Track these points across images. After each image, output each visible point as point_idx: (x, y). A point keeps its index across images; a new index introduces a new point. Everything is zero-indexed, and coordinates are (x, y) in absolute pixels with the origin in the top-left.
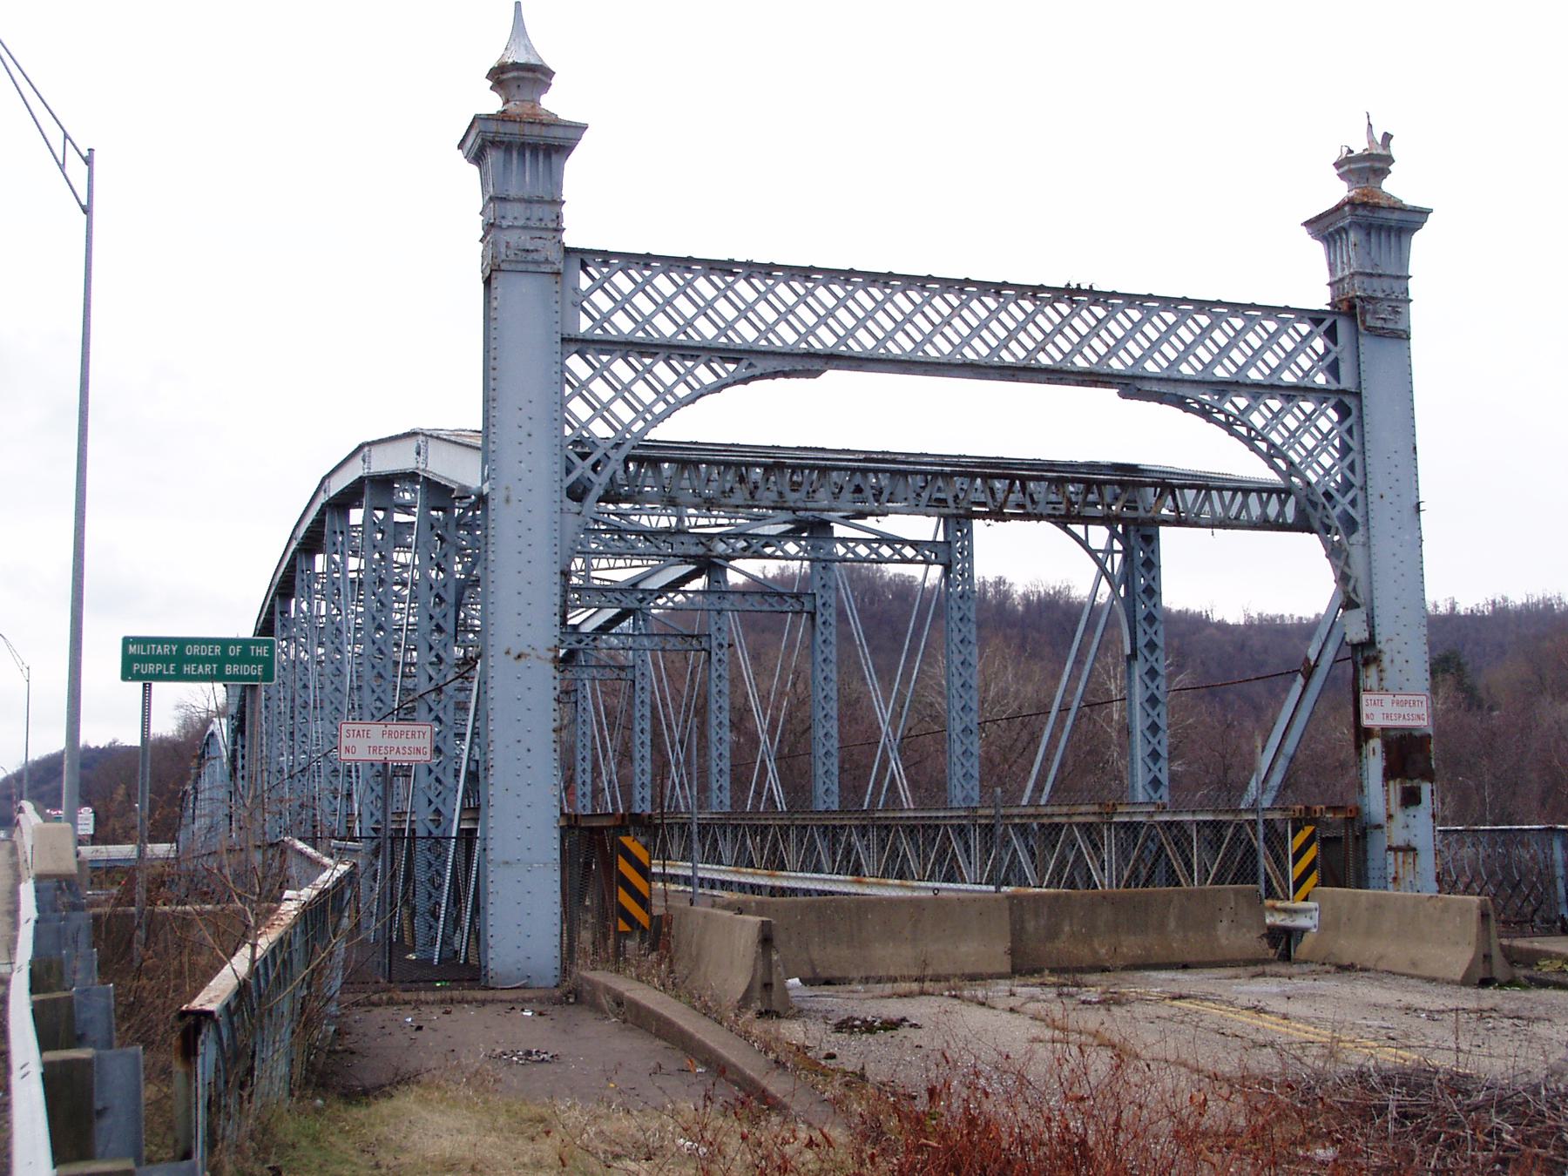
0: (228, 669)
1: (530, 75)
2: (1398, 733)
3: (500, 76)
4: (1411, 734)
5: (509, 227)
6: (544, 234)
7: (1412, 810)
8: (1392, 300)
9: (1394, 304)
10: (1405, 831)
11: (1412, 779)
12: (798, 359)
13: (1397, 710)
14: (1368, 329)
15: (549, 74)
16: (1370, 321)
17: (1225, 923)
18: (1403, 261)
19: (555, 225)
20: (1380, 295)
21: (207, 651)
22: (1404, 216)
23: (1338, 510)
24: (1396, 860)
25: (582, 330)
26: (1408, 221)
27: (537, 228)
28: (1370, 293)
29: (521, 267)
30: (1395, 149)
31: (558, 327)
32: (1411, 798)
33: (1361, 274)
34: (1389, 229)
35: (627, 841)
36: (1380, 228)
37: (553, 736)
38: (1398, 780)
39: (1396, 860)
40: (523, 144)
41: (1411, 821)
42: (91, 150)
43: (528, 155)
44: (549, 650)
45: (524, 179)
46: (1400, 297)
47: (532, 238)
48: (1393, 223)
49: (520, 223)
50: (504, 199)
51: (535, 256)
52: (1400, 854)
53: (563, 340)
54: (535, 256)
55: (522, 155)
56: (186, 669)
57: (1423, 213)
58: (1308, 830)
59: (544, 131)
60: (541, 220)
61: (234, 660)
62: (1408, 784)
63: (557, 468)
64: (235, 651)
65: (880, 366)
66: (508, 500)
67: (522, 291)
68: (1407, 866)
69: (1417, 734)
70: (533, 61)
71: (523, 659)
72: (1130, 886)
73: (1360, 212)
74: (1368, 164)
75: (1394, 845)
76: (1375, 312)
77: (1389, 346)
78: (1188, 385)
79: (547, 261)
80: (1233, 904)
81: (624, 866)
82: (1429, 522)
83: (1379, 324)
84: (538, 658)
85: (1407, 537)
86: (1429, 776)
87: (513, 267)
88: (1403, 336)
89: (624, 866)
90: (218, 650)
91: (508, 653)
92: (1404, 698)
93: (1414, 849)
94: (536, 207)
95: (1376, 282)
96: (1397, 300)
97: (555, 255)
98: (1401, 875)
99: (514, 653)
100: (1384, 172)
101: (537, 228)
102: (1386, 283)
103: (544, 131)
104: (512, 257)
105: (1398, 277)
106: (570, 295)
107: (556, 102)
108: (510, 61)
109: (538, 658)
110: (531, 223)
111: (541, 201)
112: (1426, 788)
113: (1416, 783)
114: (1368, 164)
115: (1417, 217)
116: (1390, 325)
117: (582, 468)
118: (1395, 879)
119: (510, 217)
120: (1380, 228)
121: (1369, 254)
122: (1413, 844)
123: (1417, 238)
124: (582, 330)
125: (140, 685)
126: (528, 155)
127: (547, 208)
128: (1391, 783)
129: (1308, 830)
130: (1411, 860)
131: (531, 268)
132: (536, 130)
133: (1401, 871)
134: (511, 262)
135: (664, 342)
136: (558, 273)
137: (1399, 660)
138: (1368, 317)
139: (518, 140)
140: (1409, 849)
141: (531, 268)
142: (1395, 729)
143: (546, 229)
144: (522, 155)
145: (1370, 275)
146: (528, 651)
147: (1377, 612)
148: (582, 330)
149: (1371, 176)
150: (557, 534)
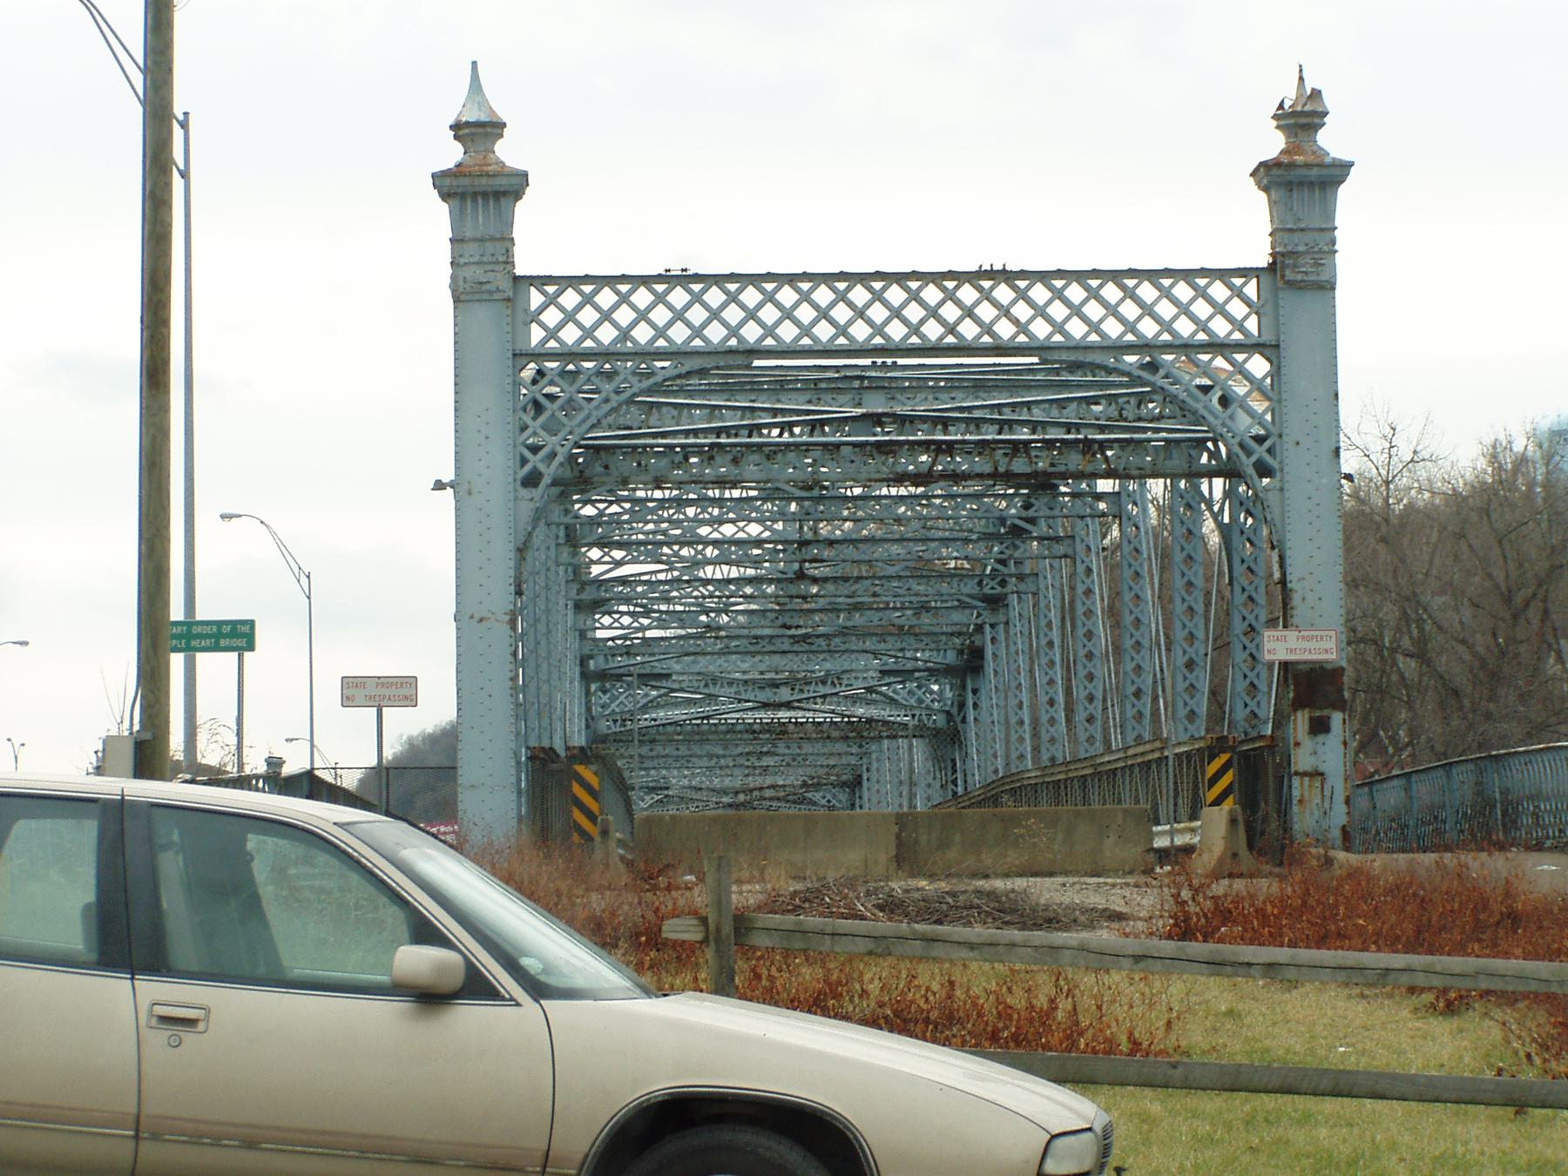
0: (223, 643)
1: (480, 130)
2: (1308, 667)
3: (461, 130)
5: (466, 264)
6: (497, 268)
7: (1321, 738)
8: (1314, 252)
9: (1317, 256)
10: (1313, 758)
11: (1321, 709)
12: (721, 356)
13: (1302, 644)
14: (1289, 283)
15: (504, 125)
16: (1289, 275)
17: (1112, 839)
18: (1329, 214)
19: (504, 259)
20: (1301, 248)
21: (208, 630)
22: (1324, 172)
23: (1253, 459)
24: (1302, 785)
25: (533, 345)
26: (1338, 172)
27: (490, 263)
28: (1290, 248)
29: (477, 297)
30: (1328, 100)
31: (509, 346)
32: (1320, 727)
33: (1281, 230)
34: (1311, 184)
35: (580, 769)
36: (1301, 184)
37: (510, 683)
38: (1307, 711)
39: (1302, 785)
40: (475, 193)
41: (1320, 749)
42: (186, 114)
43: (480, 201)
44: (505, 614)
45: (480, 222)
46: (1326, 248)
47: (485, 272)
48: (1313, 179)
49: (476, 259)
50: (462, 241)
51: (487, 287)
52: (1306, 779)
53: (514, 355)
54: (487, 287)
55: (475, 201)
56: (193, 643)
57: (1346, 167)
58: (1224, 757)
59: (491, 181)
60: (493, 255)
61: (225, 636)
62: (1318, 713)
63: (511, 463)
64: (227, 629)
65: (799, 355)
66: (470, 493)
67: (483, 314)
68: (1314, 791)
69: (1329, 667)
70: (484, 118)
71: (484, 622)
72: (1051, 805)
73: (1275, 172)
74: (1292, 121)
75: (1301, 770)
76: (1295, 266)
77: (1310, 300)
78: (1098, 351)
79: (498, 290)
80: (1120, 822)
81: (577, 790)
82: (452, 608)
83: (1299, 277)
84: (497, 620)
85: (1325, 481)
86: (1340, 705)
87: (467, 297)
88: (1329, 287)
89: (577, 790)
90: (215, 629)
91: (472, 617)
92: (1315, 633)
93: (1322, 774)
94: (487, 244)
95: (1296, 236)
96: (1320, 251)
97: (505, 284)
99: (477, 617)
100: (1316, 127)
101: (490, 263)
102: (1308, 238)
103: (491, 181)
104: (468, 289)
105: (1322, 230)
106: (521, 316)
107: (508, 152)
108: (464, 120)
109: (497, 620)
110: (485, 259)
111: (493, 239)
112: (1337, 718)
113: (1326, 712)
114: (1292, 121)
115: (1337, 171)
116: (1311, 278)
117: (535, 460)
118: (1301, 801)
119: (467, 255)
120: (1301, 184)
121: (1291, 210)
122: (1321, 769)
123: (1343, 190)
124: (533, 345)
125: (236, 654)
126: (480, 201)
127: (498, 244)
128: (1299, 714)
129: (1224, 757)
130: (1318, 784)
131: (485, 296)
132: (484, 181)
133: (1307, 794)
134: (467, 293)
135: (602, 350)
136: (508, 300)
137: (1310, 597)
138: (1287, 272)
139: (470, 190)
140: (1317, 774)
141: (485, 296)
142: (1305, 662)
143: (497, 263)
144: (475, 201)
145: (1291, 230)
146: (486, 615)
147: (1288, 553)
148: (534, 341)
149: (1299, 132)
150: (511, 518)
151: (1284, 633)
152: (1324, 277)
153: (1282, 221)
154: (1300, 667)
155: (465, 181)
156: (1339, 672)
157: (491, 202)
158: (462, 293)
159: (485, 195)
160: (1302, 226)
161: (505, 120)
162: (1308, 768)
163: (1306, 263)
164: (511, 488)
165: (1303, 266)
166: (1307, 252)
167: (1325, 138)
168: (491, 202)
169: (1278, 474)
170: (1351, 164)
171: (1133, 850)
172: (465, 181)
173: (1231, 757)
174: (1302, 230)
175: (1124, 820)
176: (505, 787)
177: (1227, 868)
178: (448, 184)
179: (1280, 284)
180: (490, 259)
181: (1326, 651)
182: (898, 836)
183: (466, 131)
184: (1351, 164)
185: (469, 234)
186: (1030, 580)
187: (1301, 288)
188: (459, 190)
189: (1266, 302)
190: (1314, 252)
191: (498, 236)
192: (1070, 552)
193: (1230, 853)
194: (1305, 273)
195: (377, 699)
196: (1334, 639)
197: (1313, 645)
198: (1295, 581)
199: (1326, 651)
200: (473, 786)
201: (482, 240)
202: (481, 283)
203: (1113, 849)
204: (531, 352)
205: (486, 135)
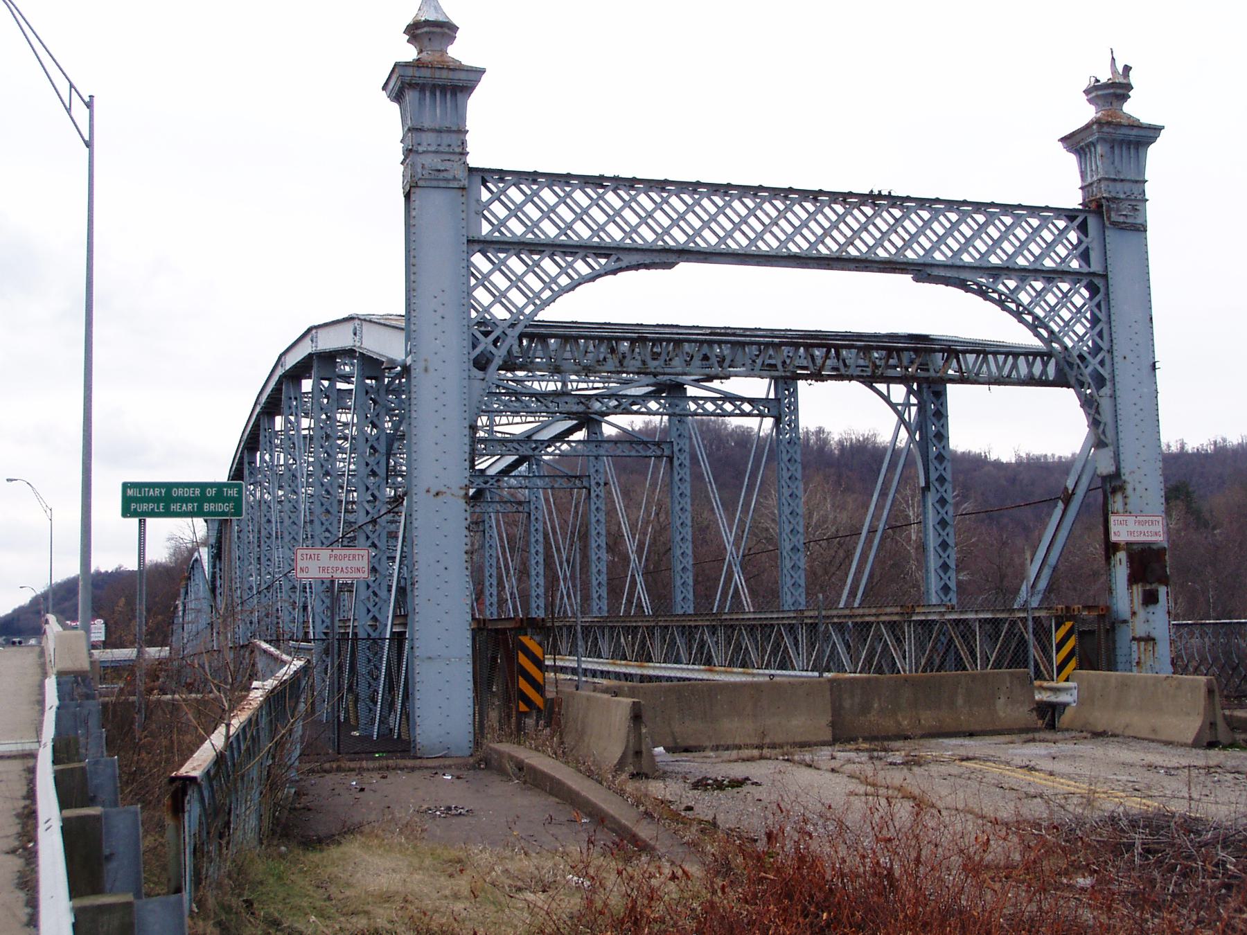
1: (438, 30)
2: (1140, 547)
4: (1149, 548)
5: (424, 152)
6: (452, 157)
7: (1151, 608)
8: (1131, 200)
9: (1134, 203)
10: (1146, 626)
11: (1151, 584)
13: (1138, 528)
14: (1114, 224)
16: (1114, 217)
17: (1002, 700)
19: (460, 150)
20: (1122, 196)
21: (189, 493)
22: (1142, 133)
24: (1139, 648)
26: (1149, 134)
28: (1114, 194)
29: (435, 183)
32: (1150, 599)
37: (465, 557)
38: (1140, 585)
39: (1139, 648)
41: (1151, 617)
43: (438, 94)
45: (434, 114)
50: (420, 130)
51: (445, 174)
54: (445, 174)
55: (433, 94)
56: (173, 507)
58: (1068, 625)
59: (451, 75)
60: (449, 146)
64: (211, 492)
65: (730, 259)
66: (426, 370)
67: (435, 202)
69: (1155, 547)
71: (440, 497)
74: (1112, 91)
75: (1138, 636)
77: (1131, 237)
79: (455, 179)
80: (1008, 685)
81: (523, 660)
83: (1121, 219)
86: (1164, 581)
88: (1141, 229)
89: (523, 660)
90: (198, 491)
91: (428, 491)
94: (444, 135)
95: (1119, 185)
96: (1136, 200)
97: (461, 174)
98: (1142, 661)
99: (433, 491)
100: (1125, 97)
102: (1127, 186)
103: (451, 75)
104: (427, 176)
108: (423, 19)
110: (441, 149)
111: (449, 131)
112: (1162, 590)
113: (1154, 586)
116: (1130, 220)
117: (485, 343)
121: (1113, 163)
126: (438, 94)
127: (454, 136)
128: (1135, 587)
130: (1151, 648)
131: (442, 184)
133: (1142, 656)
136: (463, 188)
138: (1113, 214)
140: (1149, 639)
141: (442, 184)
143: (454, 153)
145: (1114, 180)
151: (1125, 518)
152: (1139, 221)
153: (1106, 173)
154: (1135, 547)
155: (426, 73)
156: (1161, 552)
157: (449, 96)
158: (420, 179)
159: (434, 88)
160: (1122, 177)
161: (456, 22)
162: (1143, 635)
163: (1125, 208)
164: (465, 366)
165: (1124, 210)
166: (1126, 199)
167: (1130, 108)
168: (449, 96)
169: (1108, 383)
170: (1163, 128)
171: (1021, 710)
172: (426, 73)
173: (1073, 626)
174: (1122, 180)
175: (1011, 683)
176: (460, 659)
177: (1207, 738)
178: (411, 74)
179: (1107, 223)
180: (447, 149)
181: (1156, 534)
182: (1225, 748)
183: (425, 29)
184: (1163, 128)
185: (427, 124)
186: (525, 505)
187: (1122, 229)
188: (420, 82)
189: (1093, 239)
190: (1131, 200)
191: (454, 128)
192: (587, 485)
193: (1208, 723)
194: (1126, 216)
195: (330, 570)
196: (366, 558)
197: (1146, 528)
198: (1127, 474)
199: (1156, 534)
200: (430, 658)
201: (440, 131)
202: (439, 171)
203: (1009, 710)
204: (482, 239)
205: (443, 34)
